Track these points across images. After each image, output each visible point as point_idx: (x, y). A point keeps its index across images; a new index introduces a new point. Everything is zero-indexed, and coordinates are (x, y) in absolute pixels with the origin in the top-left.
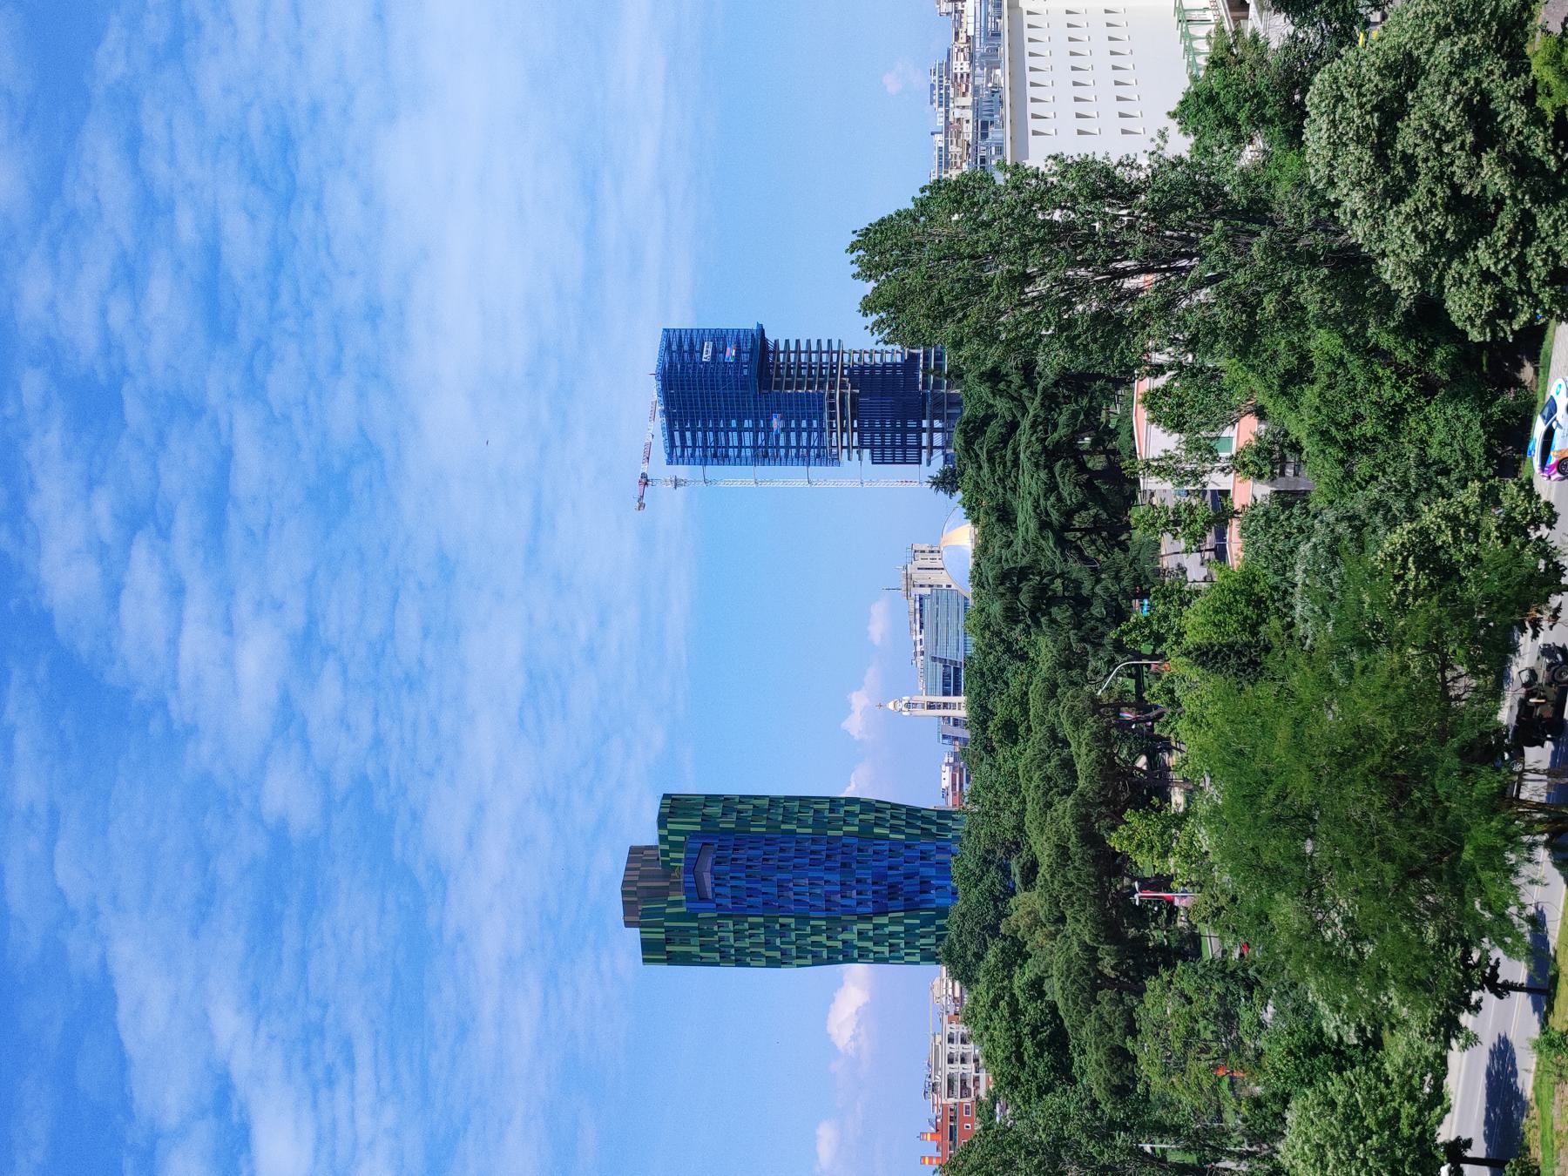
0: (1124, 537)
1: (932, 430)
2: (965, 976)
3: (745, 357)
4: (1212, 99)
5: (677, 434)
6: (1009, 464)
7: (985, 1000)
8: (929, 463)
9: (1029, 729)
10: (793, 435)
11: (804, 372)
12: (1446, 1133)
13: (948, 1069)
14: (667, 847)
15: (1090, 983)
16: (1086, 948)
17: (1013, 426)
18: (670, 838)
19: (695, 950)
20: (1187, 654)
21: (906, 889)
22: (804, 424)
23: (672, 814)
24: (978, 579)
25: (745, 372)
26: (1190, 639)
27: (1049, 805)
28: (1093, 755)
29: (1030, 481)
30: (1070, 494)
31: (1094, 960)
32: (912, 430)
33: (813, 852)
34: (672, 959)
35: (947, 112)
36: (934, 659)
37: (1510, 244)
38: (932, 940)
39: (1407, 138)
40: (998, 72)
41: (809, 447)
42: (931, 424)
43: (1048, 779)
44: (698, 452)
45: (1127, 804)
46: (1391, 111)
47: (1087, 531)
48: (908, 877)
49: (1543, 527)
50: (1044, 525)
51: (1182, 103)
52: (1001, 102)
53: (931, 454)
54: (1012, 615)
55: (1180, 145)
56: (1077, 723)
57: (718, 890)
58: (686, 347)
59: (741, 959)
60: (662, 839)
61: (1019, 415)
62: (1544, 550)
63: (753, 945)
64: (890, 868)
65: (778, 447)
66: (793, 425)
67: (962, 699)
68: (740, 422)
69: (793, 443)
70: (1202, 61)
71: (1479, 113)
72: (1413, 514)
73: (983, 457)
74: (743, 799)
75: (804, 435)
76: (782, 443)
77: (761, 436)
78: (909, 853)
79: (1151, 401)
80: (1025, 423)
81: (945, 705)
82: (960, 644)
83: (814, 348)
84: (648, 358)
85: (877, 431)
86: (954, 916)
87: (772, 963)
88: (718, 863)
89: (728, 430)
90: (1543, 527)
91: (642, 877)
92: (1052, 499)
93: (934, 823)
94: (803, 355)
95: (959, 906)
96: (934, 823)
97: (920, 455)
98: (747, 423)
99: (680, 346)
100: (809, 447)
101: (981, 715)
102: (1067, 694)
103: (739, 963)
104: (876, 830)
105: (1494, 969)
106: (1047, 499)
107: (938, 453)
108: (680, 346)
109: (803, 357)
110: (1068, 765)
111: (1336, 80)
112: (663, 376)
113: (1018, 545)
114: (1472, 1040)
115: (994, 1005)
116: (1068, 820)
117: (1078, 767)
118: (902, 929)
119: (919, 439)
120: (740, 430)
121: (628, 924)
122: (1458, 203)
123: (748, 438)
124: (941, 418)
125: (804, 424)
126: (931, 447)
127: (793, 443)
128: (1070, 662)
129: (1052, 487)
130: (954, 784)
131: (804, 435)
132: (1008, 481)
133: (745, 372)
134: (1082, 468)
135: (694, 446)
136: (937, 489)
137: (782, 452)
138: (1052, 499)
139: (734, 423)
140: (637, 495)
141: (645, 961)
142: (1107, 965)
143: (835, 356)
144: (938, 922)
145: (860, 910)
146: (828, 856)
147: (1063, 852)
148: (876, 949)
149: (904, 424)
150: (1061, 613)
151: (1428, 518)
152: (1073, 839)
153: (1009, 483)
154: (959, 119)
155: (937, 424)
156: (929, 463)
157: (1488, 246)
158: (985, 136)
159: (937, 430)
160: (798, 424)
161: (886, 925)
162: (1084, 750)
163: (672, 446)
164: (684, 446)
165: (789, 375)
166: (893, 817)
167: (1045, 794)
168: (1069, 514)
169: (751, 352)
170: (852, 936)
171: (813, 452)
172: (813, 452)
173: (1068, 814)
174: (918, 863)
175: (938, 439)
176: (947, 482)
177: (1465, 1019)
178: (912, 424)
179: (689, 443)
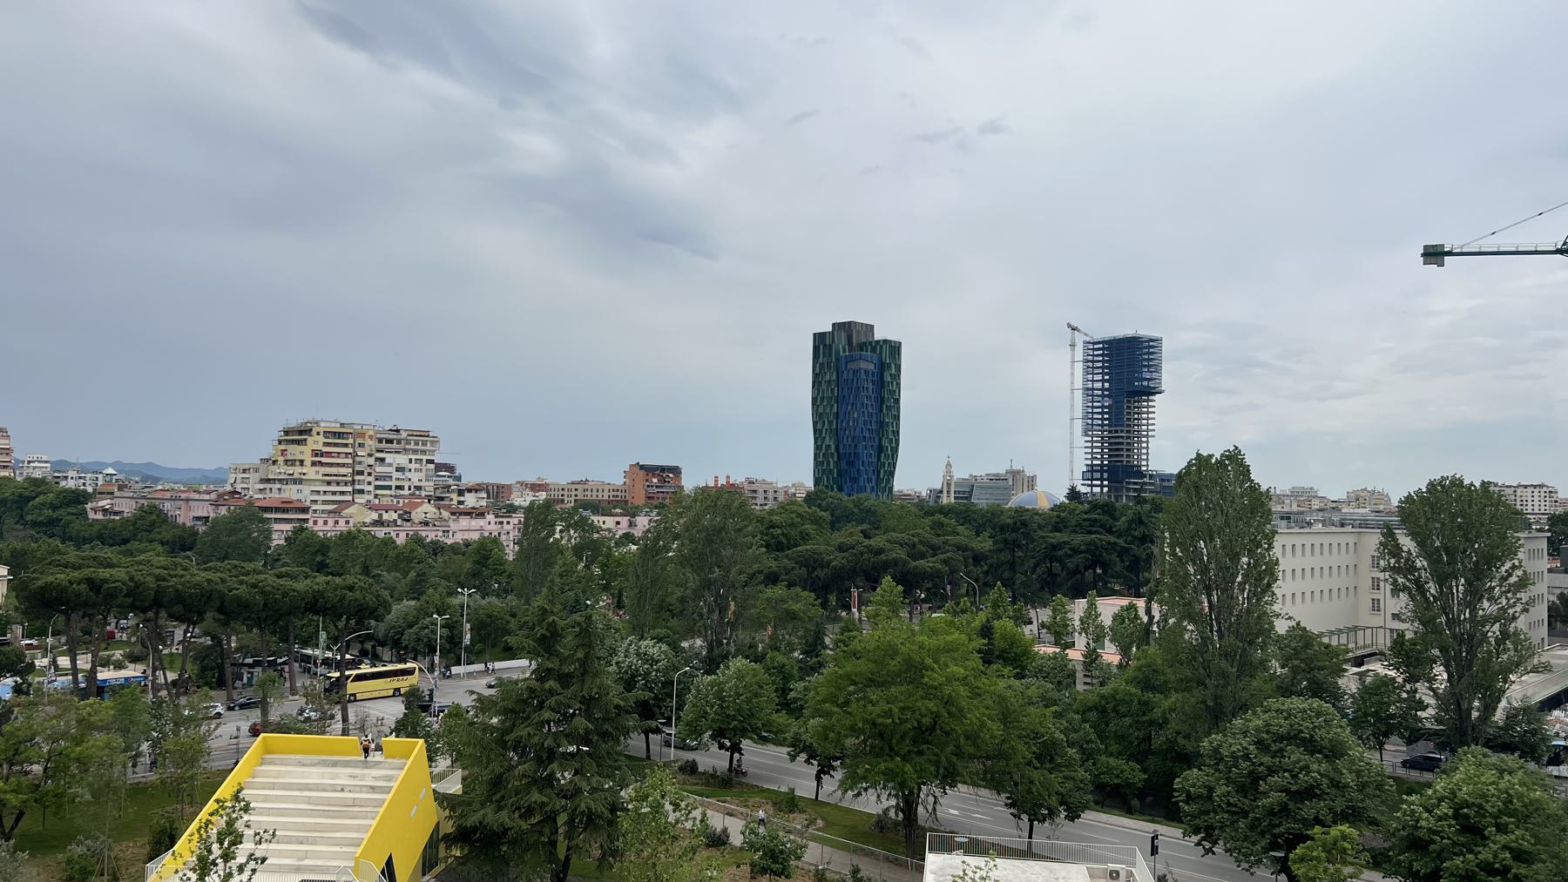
0: (1046, 589)
1: (1102, 486)
2: (810, 498)
3: (1145, 383)
4: (1308, 645)
5: (1101, 346)
6: (1089, 529)
7: (800, 510)
8: (1083, 485)
9: (939, 535)
10: (1100, 410)
11: (1136, 416)
12: (746, 744)
13: (761, 491)
14: (873, 344)
15: (812, 563)
16: (828, 563)
17: (1110, 531)
18: (878, 347)
19: (821, 360)
20: (988, 621)
21: (852, 470)
22: (1106, 416)
23: (891, 347)
24: (1020, 511)
25: (1136, 383)
26: (996, 623)
27: (901, 545)
28: (929, 569)
29: (1079, 539)
30: (1071, 562)
31: (822, 567)
32: (1102, 475)
33: (871, 422)
34: (816, 349)
35: (1288, 496)
36: (973, 486)
37: (1229, 804)
38: (826, 483)
39: (1295, 755)
40: (1321, 525)
41: (1092, 419)
42: (1105, 486)
43: (914, 546)
44: (1091, 358)
45: (665, 520)
46: (1311, 746)
47: (1050, 570)
48: (858, 470)
49: (1066, 813)
50: (1055, 547)
51: (1305, 628)
52: (1302, 528)
53: (1088, 485)
54: (1003, 528)
55: (1281, 627)
56: (945, 562)
57: (851, 372)
58: (1151, 350)
59: (816, 383)
60: (878, 342)
61: (1116, 534)
62: (1052, 814)
63: (823, 391)
64: (863, 462)
65: (1093, 402)
66: (1105, 410)
67: (953, 501)
68: (1107, 381)
69: (1095, 410)
70: (1325, 640)
71: (1309, 793)
72: (1071, 744)
73: (1093, 516)
74: (898, 385)
75: (1100, 416)
76: (1095, 404)
77: (1100, 393)
78: (870, 472)
79: (1132, 607)
80: (1112, 539)
81: (948, 492)
82: (981, 501)
83: (1150, 422)
84: (1144, 332)
85: (1102, 456)
86: (839, 495)
87: (814, 400)
88: (865, 371)
89: (1103, 374)
90: (1066, 813)
91: (858, 332)
92: (1069, 552)
93: (886, 485)
94: (1146, 415)
95: (846, 498)
96: (886, 485)
97: (1088, 480)
98: (1107, 385)
99: (1153, 347)
100: (1092, 419)
101: (946, 511)
102: (959, 556)
103: (814, 383)
104: (883, 455)
105: (828, 773)
106: (1070, 549)
107: (1088, 489)
108: (1153, 347)
109: (1145, 416)
110: (922, 556)
111: (1328, 714)
112: (1135, 337)
113: (1040, 533)
114: (793, 758)
115: (800, 515)
116: (895, 555)
117: (922, 561)
118: (832, 467)
119: (1097, 480)
120: (1103, 381)
121: (834, 325)
122: (1255, 778)
123: (1099, 385)
124: (1109, 491)
125: (1106, 416)
126: (1092, 486)
127: (1095, 410)
128: (978, 558)
129: (1076, 551)
130: (904, 495)
131: (1100, 416)
132: (1078, 528)
133: (1136, 383)
134: (1087, 568)
135: (1093, 355)
136: (1070, 489)
137: (1090, 404)
138: (1069, 552)
139: (1107, 377)
140: (1082, 329)
141: (815, 334)
142: (821, 573)
143: (1145, 433)
144: (835, 486)
145: (841, 447)
146: (869, 429)
147: (880, 552)
148: (821, 454)
149: (1106, 471)
150: (1006, 556)
151: (1072, 752)
152: (885, 558)
153: (1077, 529)
154: (1283, 502)
155: (1105, 489)
156: (1083, 485)
157: (1229, 792)
158: (1282, 518)
159: (1102, 490)
160: (1106, 413)
161: (833, 459)
162: (931, 565)
163: (1094, 343)
164: (1094, 349)
165: (1135, 407)
166: (889, 463)
167: (906, 544)
168: (1060, 561)
169: (1148, 387)
170: (827, 442)
171: (1090, 421)
172: (1090, 421)
173: (898, 556)
174: (866, 477)
175: (1096, 490)
176: (1073, 494)
177: (803, 756)
178: (1105, 475)
179: (1096, 353)
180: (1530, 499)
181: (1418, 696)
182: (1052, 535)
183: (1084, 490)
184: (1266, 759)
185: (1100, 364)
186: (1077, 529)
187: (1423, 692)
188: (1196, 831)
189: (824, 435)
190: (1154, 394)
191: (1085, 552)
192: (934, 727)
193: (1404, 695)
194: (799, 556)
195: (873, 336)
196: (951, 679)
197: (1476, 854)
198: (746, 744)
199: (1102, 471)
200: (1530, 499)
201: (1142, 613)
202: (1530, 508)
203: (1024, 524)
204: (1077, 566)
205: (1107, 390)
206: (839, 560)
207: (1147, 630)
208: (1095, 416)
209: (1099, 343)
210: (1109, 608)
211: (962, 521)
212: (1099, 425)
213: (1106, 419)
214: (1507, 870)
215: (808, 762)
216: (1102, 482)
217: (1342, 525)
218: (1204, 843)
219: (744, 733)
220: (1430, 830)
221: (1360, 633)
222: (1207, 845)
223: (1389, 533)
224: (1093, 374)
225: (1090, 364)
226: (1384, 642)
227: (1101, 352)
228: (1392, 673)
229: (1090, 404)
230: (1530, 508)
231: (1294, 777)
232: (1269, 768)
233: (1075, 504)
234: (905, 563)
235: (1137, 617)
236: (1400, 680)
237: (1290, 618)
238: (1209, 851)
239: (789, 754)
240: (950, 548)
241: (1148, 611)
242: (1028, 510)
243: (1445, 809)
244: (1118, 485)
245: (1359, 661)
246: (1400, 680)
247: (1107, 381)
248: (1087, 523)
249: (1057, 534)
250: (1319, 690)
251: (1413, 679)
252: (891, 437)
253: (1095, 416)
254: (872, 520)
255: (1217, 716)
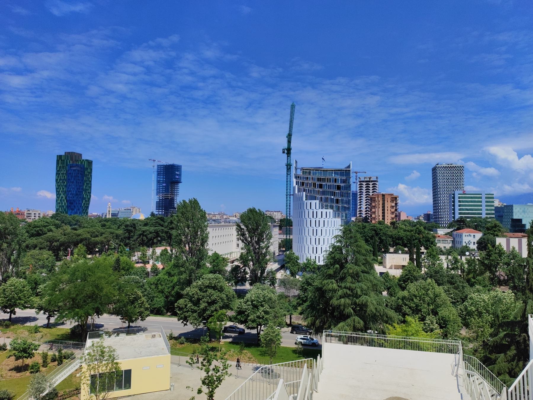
0: (141, 246)
1: (162, 212)
3: (176, 179)
4: (218, 258)
13: (33, 213)
14: (82, 161)
15: (51, 241)
17: (162, 226)
18: (83, 162)
19: (60, 165)
20: (118, 257)
22: (164, 189)
26: (121, 258)
29: (152, 229)
31: (56, 241)
32: (162, 208)
36: (118, 212)
37: (192, 309)
38: (61, 211)
46: (214, 288)
47: (142, 239)
50: (144, 232)
54: (127, 226)
55: (210, 253)
56: (105, 238)
60: (83, 160)
64: (76, 203)
67: (110, 217)
68: (164, 178)
70: (224, 256)
74: (91, 176)
77: (162, 182)
79: (166, 250)
82: (121, 216)
86: (66, 215)
89: (163, 176)
92: (149, 233)
98: (164, 179)
99: (179, 168)
100: (160, 190)
102: (111, 236)
108: (179, 168)
109: (176, 190)
110: (97, 236)
113: (140, 227)
115: (47, 222)
116: (85, 236)
120: (163, 178)
123: (162, 179)
126: (159, 212)
128: (117, 236)
129: (151, 233)
134: (154, 238)
135: (160, 170)
137: (159, 185)
138: (149, 233)
139: (164, 177)
142: (55, 244)
144: (65, 212)
147: (79, 235)
149: (163, 207)
150: (127, 235)
151: (143, 299)
153: (152, 225)
155: (163, 213)
157: (191, 305)
158: (213, 221)
161: (64, 202)
162: (100, 239)
163: (161, 166)
168: (146, 236)
169: (177, 181)
170: (62, 195)
172: (159, 191)
175: (160, 213)
176: (153, 214)
177: (42, 312)
178: (163, 208)
180: (277, 215)
181: (246, 270)
182: (143, 227)
183: (156, 213)
184: (202, 294)
185: (162, 173)
186: (152, 225)
187: (248, 270)
188: (181, 319)
189: (60, 193)
190: (179, 183)
191: (154, 233)
192: (531, 258)
193: (467, 253)
194: (47, 238)
195: (81, 157)
196: (100, 278)
197: (256, 314)
198: (17, 310)
199: (162, 207)
200: (277, 215)
201: (169, 251)
202: (277, 217)
203: (134, 224)
204: (151, 237)
205: (164, 181)
206: (63, 239)
207: (171, 257)
208: (161, 189)
209: (162, 166)
210: (159, 250)
211: (113, 224)
212: (161, 192)
213: (164, 190)
214: (263, 317)
215: (44, 313)
216: (439, 200)
217: (229, 223)
218: (184, 322)
219: (16, 305)
220: (245, 308)
221: (233, 254)
222: (185, 323)
223: (238, 226)
224: (160, 176)
225: (159, 172)
226: (238, 256)
227: (163, 169)
228: (240, 265)
229: (159, 185)
230: (277, 217)
231: (210, 298)
232: (203, 296)
233: (152, 218)
234: (89, 239)
235: (167, 252)
236: (241, 266)
237: (212, 250)
238: (185, 324)
239: (36, 312)
240: (108, 233)
241: (172, 251)
242: (137, 220)
243: (250, 303)
244: (167, 211)
245: (233, 262)
246: (241, 266)
247: (164, 178)
248: (154, 224)
249: (145, 227)
250: (220, 272)
251: (245, 266)
252: (88, 194)
253: (161, 189)
254: (78, 224)
255: (189, 283)
